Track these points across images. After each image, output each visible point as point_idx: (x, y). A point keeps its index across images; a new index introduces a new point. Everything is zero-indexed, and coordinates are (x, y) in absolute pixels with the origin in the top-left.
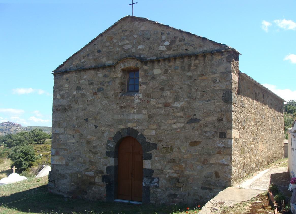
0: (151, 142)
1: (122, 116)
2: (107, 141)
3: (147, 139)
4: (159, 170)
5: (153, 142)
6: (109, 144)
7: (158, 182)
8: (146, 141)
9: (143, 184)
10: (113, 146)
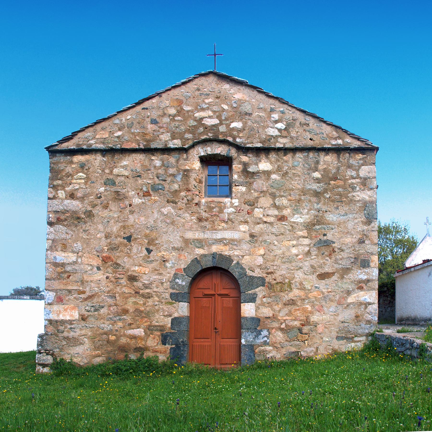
0: (256, 276)
1: (203, 233)
2: (172, 276)
3: (248, 271)
5: (259, 275)
6: (177, 280)
7: (268, 336)
8: (247, 274)
9: (242, 341)
10: (184, 283)
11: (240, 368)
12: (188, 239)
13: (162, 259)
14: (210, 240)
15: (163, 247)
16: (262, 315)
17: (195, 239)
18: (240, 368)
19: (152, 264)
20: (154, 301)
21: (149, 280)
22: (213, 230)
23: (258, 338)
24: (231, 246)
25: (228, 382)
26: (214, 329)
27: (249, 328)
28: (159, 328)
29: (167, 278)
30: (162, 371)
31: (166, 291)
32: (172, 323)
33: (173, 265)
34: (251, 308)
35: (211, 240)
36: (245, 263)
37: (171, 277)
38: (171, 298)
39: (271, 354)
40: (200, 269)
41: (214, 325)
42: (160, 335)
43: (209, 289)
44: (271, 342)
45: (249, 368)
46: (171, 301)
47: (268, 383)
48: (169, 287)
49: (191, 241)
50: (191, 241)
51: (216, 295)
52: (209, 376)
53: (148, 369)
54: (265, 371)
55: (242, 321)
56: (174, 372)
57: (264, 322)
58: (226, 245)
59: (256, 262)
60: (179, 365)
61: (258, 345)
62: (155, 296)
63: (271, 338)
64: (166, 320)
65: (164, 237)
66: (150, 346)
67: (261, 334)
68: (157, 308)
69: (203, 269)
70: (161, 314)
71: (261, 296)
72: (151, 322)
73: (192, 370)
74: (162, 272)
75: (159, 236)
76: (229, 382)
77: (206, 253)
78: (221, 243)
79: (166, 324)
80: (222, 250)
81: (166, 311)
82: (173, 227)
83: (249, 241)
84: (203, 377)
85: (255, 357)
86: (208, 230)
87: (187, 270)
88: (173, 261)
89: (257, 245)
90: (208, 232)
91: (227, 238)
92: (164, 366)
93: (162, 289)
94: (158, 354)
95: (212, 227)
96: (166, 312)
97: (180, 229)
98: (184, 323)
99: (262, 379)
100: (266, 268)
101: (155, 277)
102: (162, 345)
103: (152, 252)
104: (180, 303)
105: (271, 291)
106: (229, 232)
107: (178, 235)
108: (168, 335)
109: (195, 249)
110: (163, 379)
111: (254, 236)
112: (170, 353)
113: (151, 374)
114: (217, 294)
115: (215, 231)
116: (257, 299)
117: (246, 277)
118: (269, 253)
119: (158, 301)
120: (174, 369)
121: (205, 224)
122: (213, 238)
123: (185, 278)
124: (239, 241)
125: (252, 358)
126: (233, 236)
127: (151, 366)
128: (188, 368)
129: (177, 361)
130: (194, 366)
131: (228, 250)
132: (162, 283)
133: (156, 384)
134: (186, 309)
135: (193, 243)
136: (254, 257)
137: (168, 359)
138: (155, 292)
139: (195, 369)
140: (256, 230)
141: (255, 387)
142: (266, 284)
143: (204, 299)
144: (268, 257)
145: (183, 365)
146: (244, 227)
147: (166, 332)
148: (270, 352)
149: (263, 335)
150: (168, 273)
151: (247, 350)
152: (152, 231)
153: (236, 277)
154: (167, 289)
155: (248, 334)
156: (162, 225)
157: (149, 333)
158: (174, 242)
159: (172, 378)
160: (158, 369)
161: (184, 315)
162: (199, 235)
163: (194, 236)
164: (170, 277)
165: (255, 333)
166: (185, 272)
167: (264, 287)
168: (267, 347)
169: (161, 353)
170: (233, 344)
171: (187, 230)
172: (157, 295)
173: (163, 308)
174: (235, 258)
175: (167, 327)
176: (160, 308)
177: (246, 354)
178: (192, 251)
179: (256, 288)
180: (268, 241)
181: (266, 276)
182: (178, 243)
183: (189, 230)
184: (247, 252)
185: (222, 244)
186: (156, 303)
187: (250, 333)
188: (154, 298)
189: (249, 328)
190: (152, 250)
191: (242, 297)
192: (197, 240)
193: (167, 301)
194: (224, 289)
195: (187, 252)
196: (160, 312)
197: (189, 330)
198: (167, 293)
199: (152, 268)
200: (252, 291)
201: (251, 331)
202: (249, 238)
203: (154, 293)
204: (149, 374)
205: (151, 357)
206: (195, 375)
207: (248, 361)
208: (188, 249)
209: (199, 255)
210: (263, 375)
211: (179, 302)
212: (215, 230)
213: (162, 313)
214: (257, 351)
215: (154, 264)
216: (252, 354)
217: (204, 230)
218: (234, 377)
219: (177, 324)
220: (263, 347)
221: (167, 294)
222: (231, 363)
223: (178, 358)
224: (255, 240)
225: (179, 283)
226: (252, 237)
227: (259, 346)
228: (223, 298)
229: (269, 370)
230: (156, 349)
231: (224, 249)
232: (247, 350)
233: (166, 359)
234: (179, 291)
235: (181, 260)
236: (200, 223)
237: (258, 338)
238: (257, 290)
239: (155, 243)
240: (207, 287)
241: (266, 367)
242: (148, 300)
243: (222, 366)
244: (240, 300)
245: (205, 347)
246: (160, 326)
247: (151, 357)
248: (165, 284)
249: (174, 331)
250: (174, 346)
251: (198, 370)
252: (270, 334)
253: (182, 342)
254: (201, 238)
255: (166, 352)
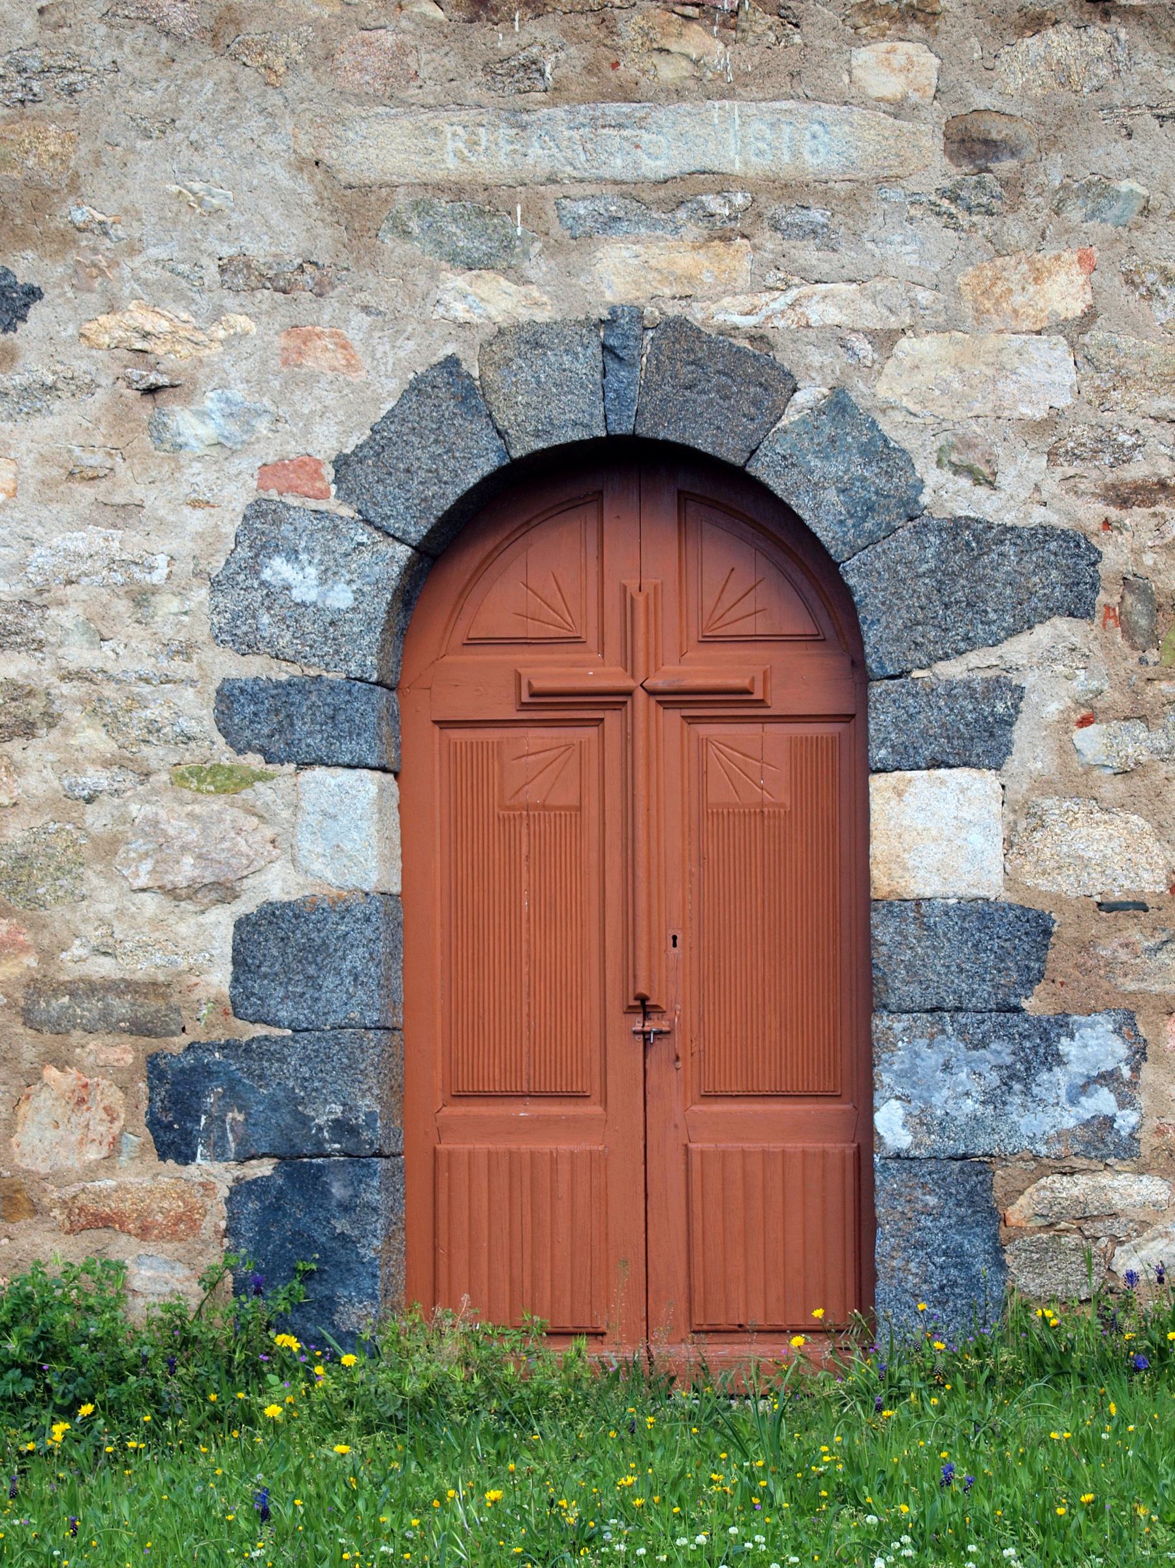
0: (1009, 519)
1: (505, 131)
2: (230, 529)
3: (933, 477)
4: (1143, 907)
5: (1039, 516)
6: (278, 569)
7: (1126, 1072)
8: (925, 499)
9: (880, 1119)
10: (341, 597)
11: (861, 1368)
12: (367, 189)
13: (135, 373)
14: (576, 190)
15: (138, 261)
16: (1065, 885)
17: (439, 188)
18: (861, 1368)
19: (37, 421)
20: (69, 764)
21: (22, 566)
22: (605, 97)
23: (1027, 1092)
24: (770, 242)
25: (767, 1494)
26: (630, 1010)
27: (951, 1001)
28: (121, 1007)
29: (183, 545)
30: (155, 1397)
31: (179, 668)
32: (239, 961)
33: (233, 428)
34: (966, 813)
35: (590, 189)
36: (907, 403)
37: (220, 537)
38: (225, 732)
39: (1160, 1244)
40: (486, 465)
41: (629, 972)
42: (132, 1070)
43: (576, 641)
44: (1159, 1132)
45: (948, 1375)
46: (224, 754)
47: (1134, 1518)
48: (202, 633)
49: (402, 199)
50: (402, 199)
51: (640, 695)
52: (596, 1441)
53: (29, 1384)
54: (1100, 1408)
55: (884, 933)
56: (273, 1411)
57: (1085, 946)
58: (726, 239)
59: (1008, 388)
60: (321, 1342)
61: (1036, 1158)
62: (74, 715)
63: (1156, 1094)
64: (183, 929)
65: (140, 169)
66: (43, 1168)
67: (1059, 1059)
68: (97, 818)
69: (516, 463)
70: (142, 882)
71: (1053, 709)
72: (47, 956)
73: (436, 1390)
74: (139, 493)
75: (98, 163)
76: (780, 1496)
77: (542, 316)
78: (681, 214)
79: (183, 965)
80: (690, 279)
81: (184, 849)
82: (223, 68)
83: (942, 193)
84: (533, 1448)
85: (1002, 1266)
86: (557, 92)
87: (365, 472)
88: (238, 392)
89: (1015, 231)
90: (559, 112)
91: (737, 168)
92: (181, 1357)
93: (145, 648)
94: (122, 1248)
95: (590, 69)
96: (188, 860)
97: (289, 92)
98: (355, 958)
99: (1071, 1482)
100: (1104, 442)
101: (83, 540)
102: (152, 1157)
103: (37, 312)
104: (307, 775)
105: (1152, 655)
106: (752, 109)
107: (271, 143)
108: (208, 1072)
109: (433, 274)
110: (169, 1473)
111: (987, 142)
112: (229, 1232)
113: (59, 1429)
114: (652, 693)
115: (626, 108)
116: (1021, 733)
117: (918, 533)
118: (1132, 300)
119: (107, 764)
120: (273, 1379)
121: (525, 39)
122: (606, 172)
123: (347, 546)
124: (852, 197)
125: (973, 1283)
126: (796, 154)
127: (56, 1353)
128: (400, 1367)
129: (298, 1307)
130: (451, 1346)
131: (744, 280)
132: (141, 597)
133: (105, 1520)
134: (370, 828)
135: (414, 226)
136: (992, 341)
137: (212, 1286)
138: (78, 675)
139: (459, 1374)
140: (1015, 83)
141: (1010, 1552)
142: (1102, 598)
143: (536, 737)
144: (1126, 341)
145: (349, 1340)
146: (899, 60)
147: (183, 1040)
148: (1145, 1225)
149: (1074, 1068)
150: (195, 504)
151: (932, 1201)
152: (31, 109)
153: (824, 536)
154: (185, 651)
155: (932, 1058)
156: (116, 54)
157: (29, 1053)
158: (236, 218)
159: (250, 1459)
160: (123, 1379)
161: (352, 881)
162: (473, 144)
163: (429, 152)
164: (208, 539)
165: (1001, 1051)
166: (347, 496)
167: (1081, 625)
168: (1120, 1181)
169: (144, 1232)
170: (795, 1146)
171: (362, 99)
172: (96, 709)
173: (155, 823)
174: (816, 358)
175: (200, 993)
176: (125, 819)
177: (921, 1245)
178: (411, 296)
179: (1013, 632)
180: (1124, 186)
181: (1107, 524)
182: (275, 218)
183: (376, 99)
184: (924, 296)
185: (694, 232)
186: (95, 778)
187: (953, 1046)
188: (66, 732)
189: (951, 1001)
190: (34, 294)
191: (881, 719)
192: (457, 191)
193: (191, 756)
194: (708, 640)
195: (366, 309)
196: (127, 862)
197: (398, 1020)
198: (192, 682)
199: (43, 460)
200: (974, 658)
201: (962, 1032)
202: (941, 162)
203: (66, 688)
204: (41, 1433)
205: (54, 1270)
206: (461, 1431)
207: (941, 1303)
208: (372, 281)
209: (479, 338)
210: (1083, 1441)
211: (303, 765)
212: (626, 92)
213: (147, 865)
214: (1019, 1211)
215: (55, 420)
216: (975, 1246)
217: (520, 101)
218: (810, 1455)
219: (287, 969)
220: (1081, 1179)
221: (190, 693)
222: (779, 1322)
223: (308, 1276)
224: (1005, 184)
225: (297, 595)
226: (971, 156)
227: (1042, 1166)
228: (704, 730)
229: (1144, 1400)
230: (99, 1196)
231: (707, 278)
232: (932, 1201)
233: (194, 1295)
234: (295, 670)
235: (313, 378)
236: (480, 33)
237: (1027, 1092)
238: (1017, 649)
239: (59, 223)
240: (553, 631)
241: (1105, 1366)
242: (18, 755)
243: (717, 1351)
244: (864, 740)
245: (554, 1171)
246: (128, 987)
247: (54, 1270)
248: (168, 605)
249: (260, 1030)
250: (263, 1168)
251: (487, 1384)
252: (1140, 1054)
253: (341, 1127)
254: (488, 179)
255: (194, 1226)
